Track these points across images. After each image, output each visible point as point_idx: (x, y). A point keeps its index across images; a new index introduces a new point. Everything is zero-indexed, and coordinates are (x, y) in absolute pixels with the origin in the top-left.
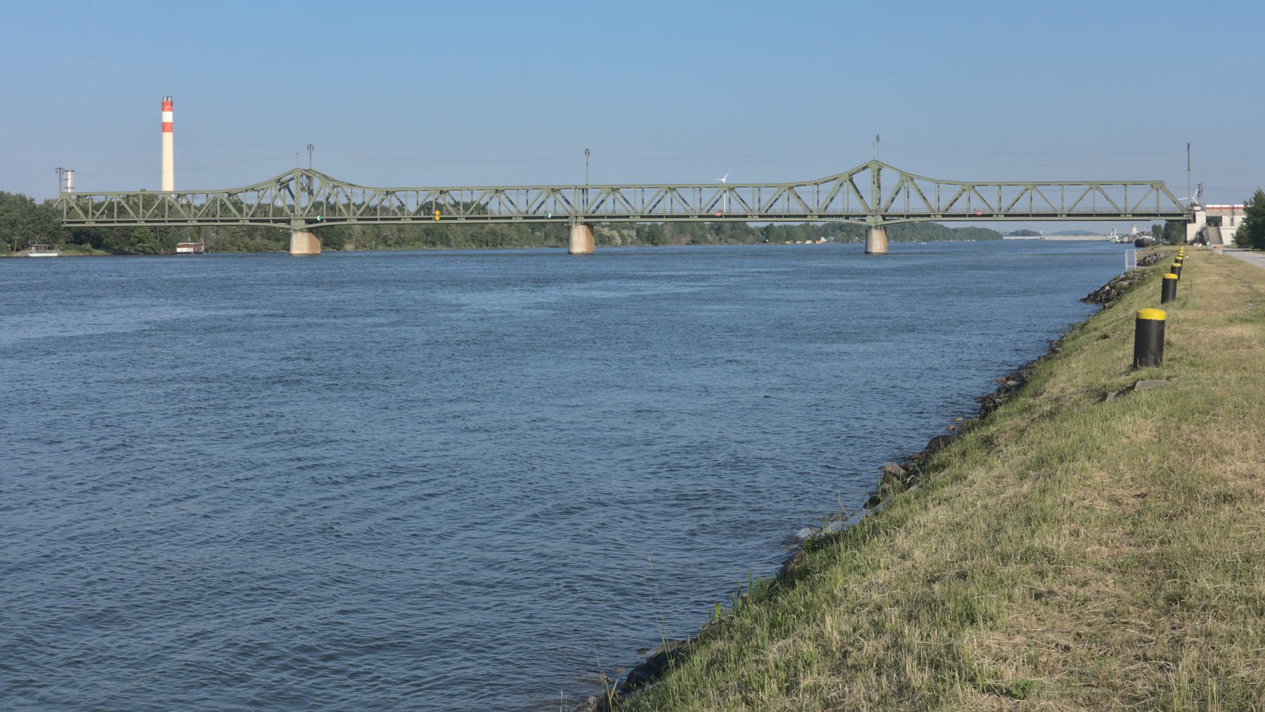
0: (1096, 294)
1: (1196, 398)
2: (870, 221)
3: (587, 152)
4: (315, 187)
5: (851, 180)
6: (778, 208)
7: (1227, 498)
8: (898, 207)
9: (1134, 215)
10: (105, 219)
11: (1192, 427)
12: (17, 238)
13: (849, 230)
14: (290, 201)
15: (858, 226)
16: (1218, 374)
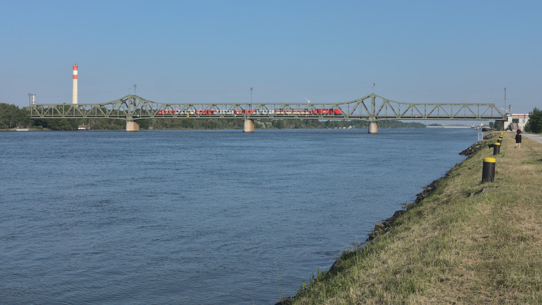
1: (509, 196)
2: (370, 119)
3: (252, 89)
4: (137, 103)
5: (363, 102)
7: (523, 239)
8: (382, 114)
11: (507, 208)
12: (11, 123)
13: (361, 123)
14: (126, 108)
16: (518, 186)
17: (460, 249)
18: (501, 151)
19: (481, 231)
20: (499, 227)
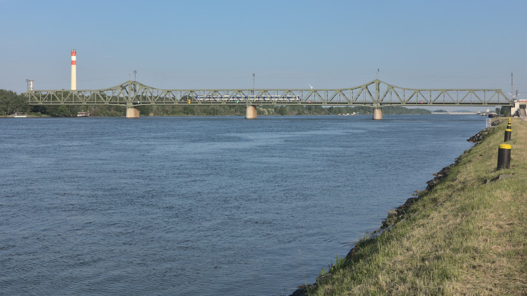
0: (474, 137)
2: (375, 105)
3: (254, 75)
4: (137, 89)
5: (367, 88)
6: (336, 100)
9: (488, 104)
10: (47, 102)
12: (9, 109)
13: (365, 110)
14: (126, 95)
15: (369, 108)
17: (487, 236)
18: (512, 138)
19: (505, 218)
20: (523, 214)
